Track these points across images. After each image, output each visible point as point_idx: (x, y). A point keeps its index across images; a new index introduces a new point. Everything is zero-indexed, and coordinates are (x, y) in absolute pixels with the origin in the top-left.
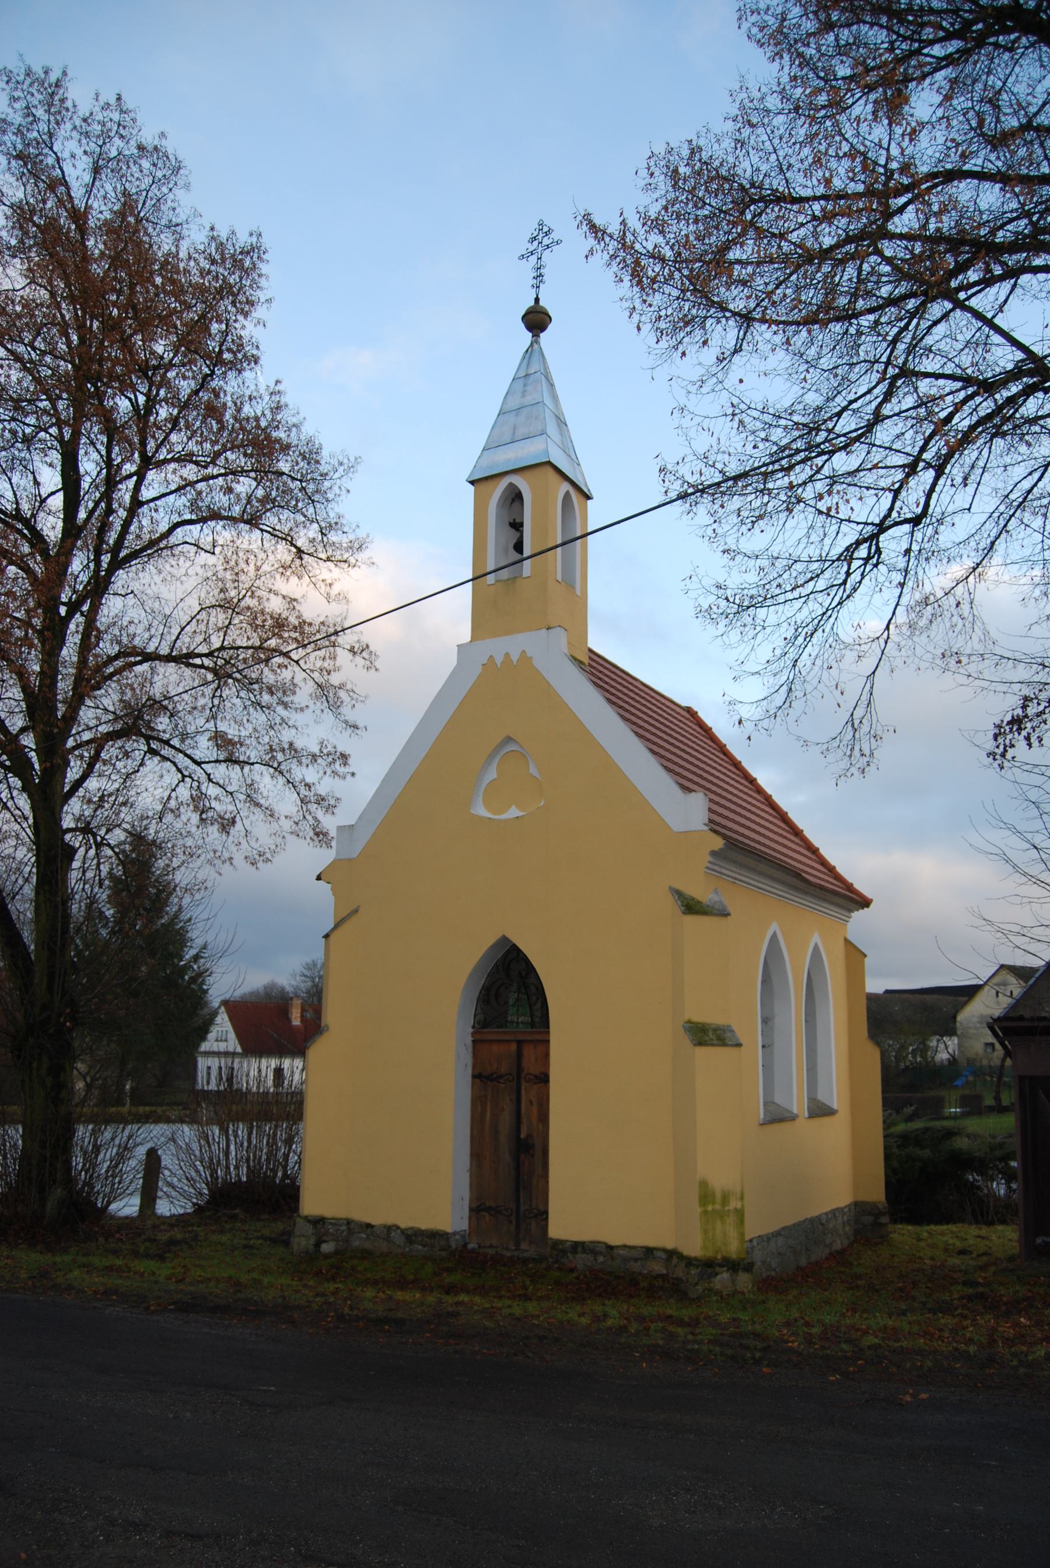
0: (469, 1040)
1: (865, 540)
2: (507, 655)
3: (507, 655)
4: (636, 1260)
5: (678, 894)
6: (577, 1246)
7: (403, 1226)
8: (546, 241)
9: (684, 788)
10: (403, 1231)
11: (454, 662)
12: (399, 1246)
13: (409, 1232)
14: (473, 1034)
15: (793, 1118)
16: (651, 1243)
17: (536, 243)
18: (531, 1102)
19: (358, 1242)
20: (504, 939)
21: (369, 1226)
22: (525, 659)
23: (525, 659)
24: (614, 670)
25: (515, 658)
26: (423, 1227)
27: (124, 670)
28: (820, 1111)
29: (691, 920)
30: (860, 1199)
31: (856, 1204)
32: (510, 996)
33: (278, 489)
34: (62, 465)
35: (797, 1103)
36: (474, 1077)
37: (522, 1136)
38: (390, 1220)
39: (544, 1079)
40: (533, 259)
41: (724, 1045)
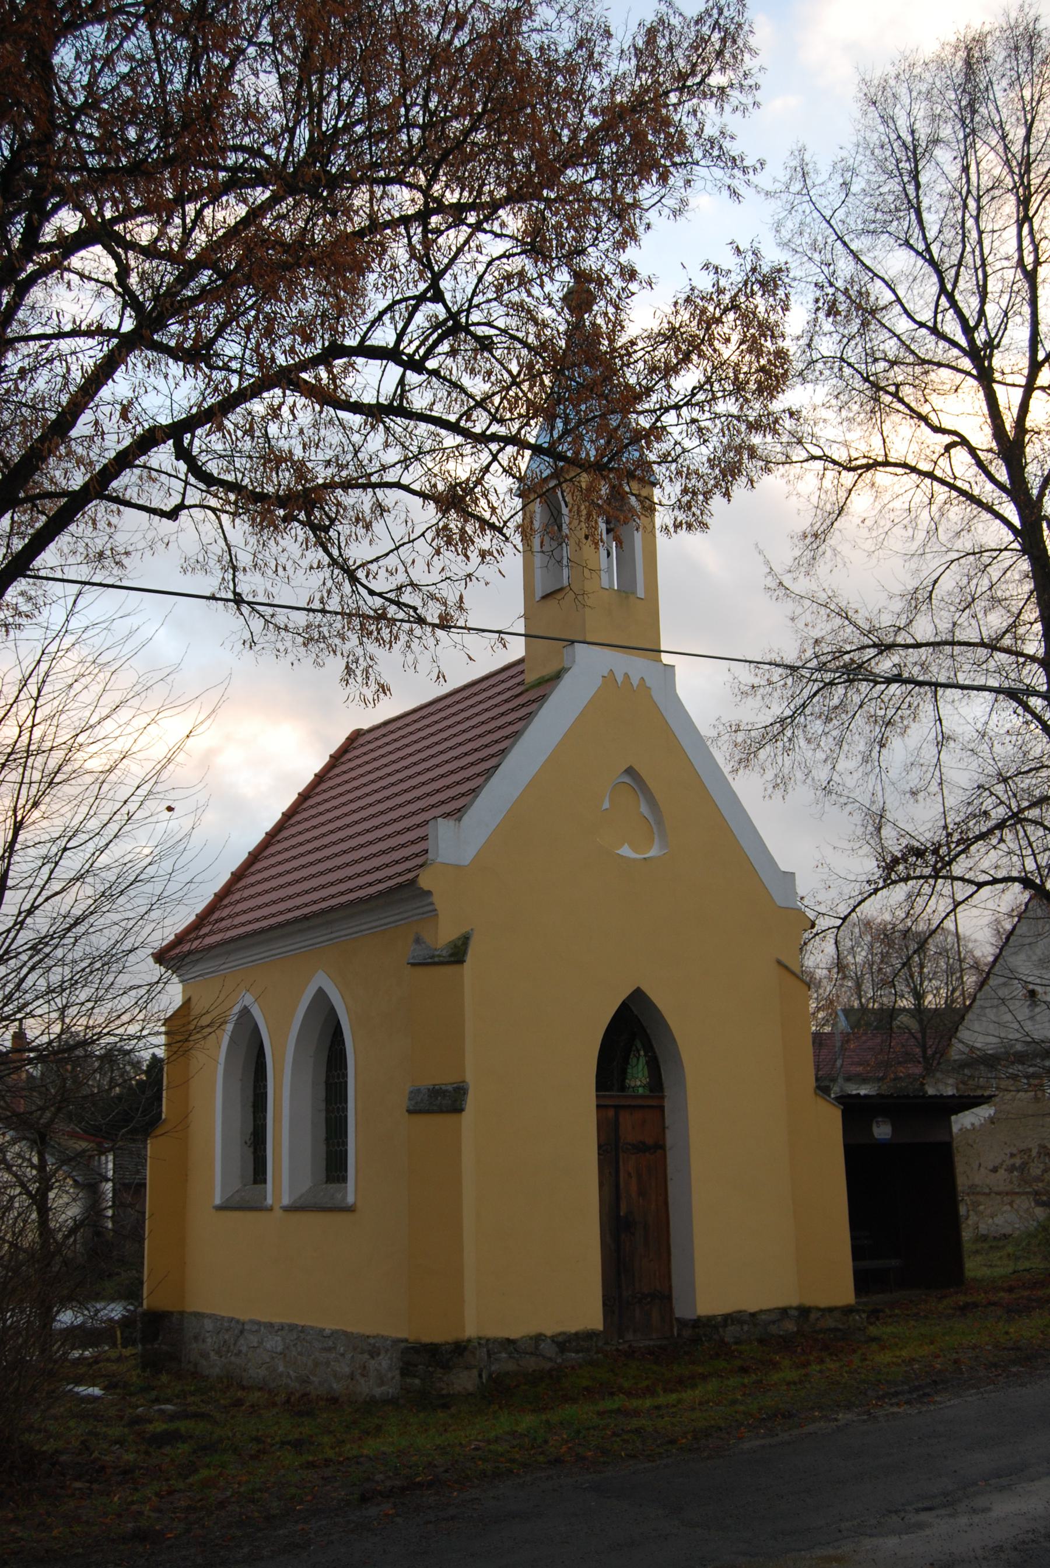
2: (626, 676)
3: (626, 676)
4: (774, 1322)
6: (729, 1319)
7: (549, 1333)
10: (553, 1339)
12: (550, 1359)
13: (560, 1339)
16: (782, 1303)
18: (629, 1174)
19: (504, 1364)
21: (509, 1341)
24: (491, 682)
25: (635, 682)
26: (573, 1330)
27: (42, 439)
32: (633, 1041)
33: (284, 318)
34: (1045, 619)
38: (532, 1329)
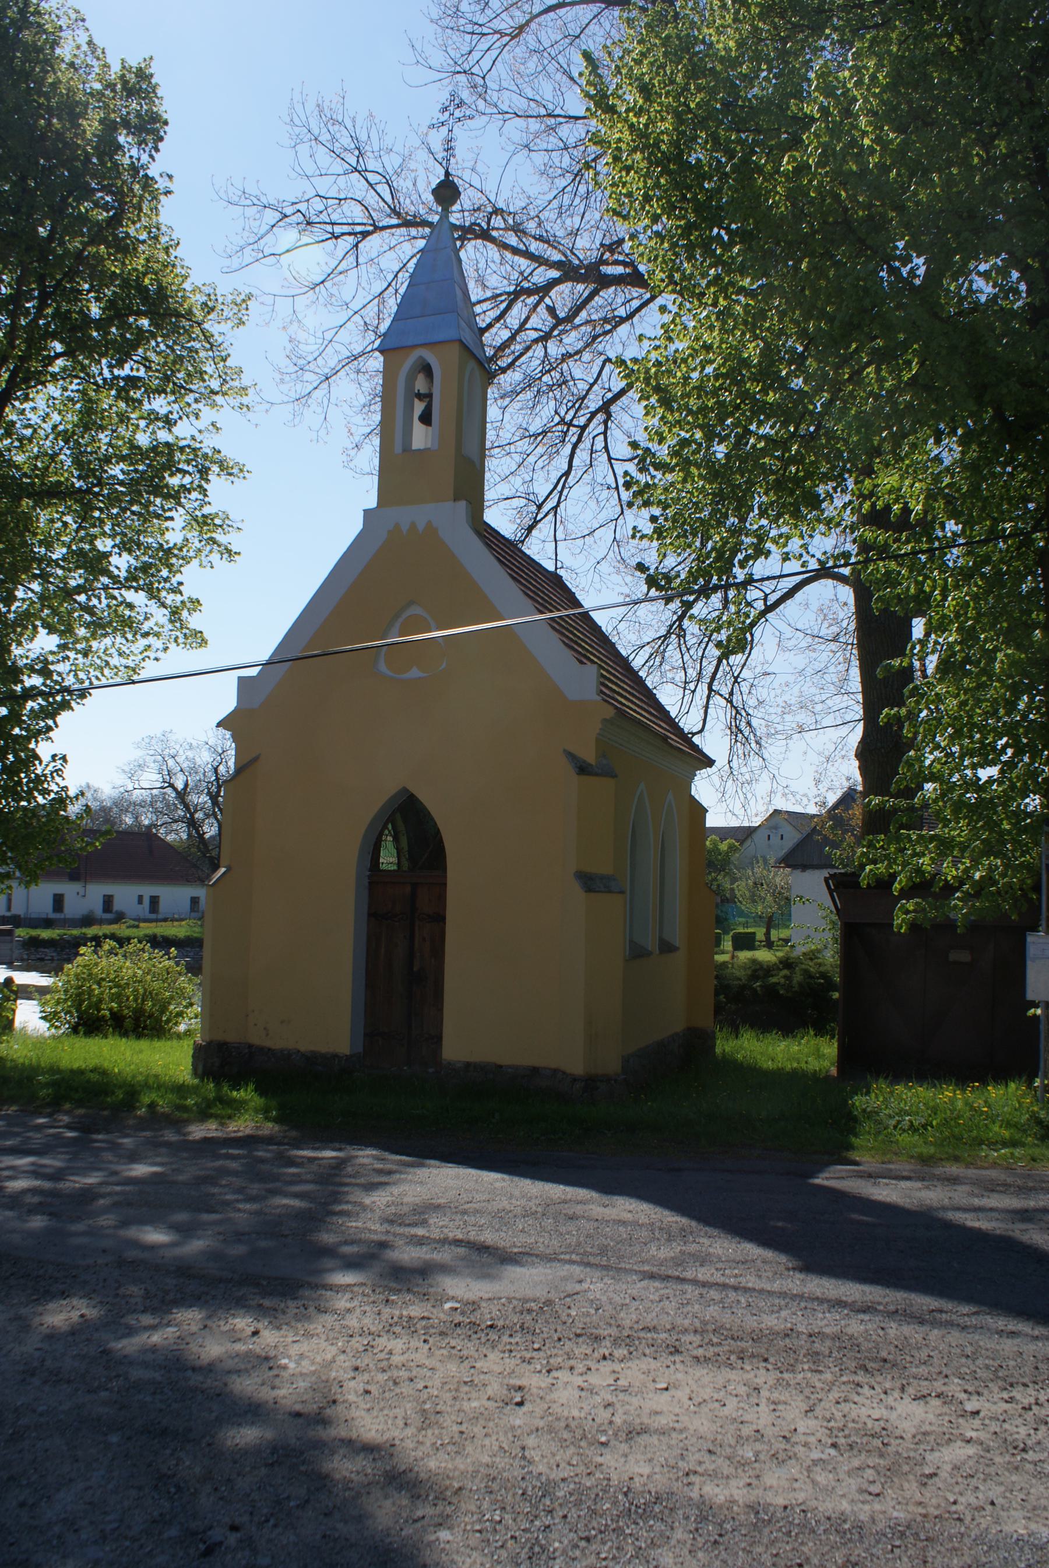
0: (366, 881)
1: (529, 292)
5: (571, 756)
8: (458, 113)
9: (581, 662)
11: (361, 527)
14: (369, 877)
15: (649, 954)
17: (447, 114)
20: (405, 790)
22: (431, 530)
23: (431, 530)
28: (667, 948)
29: (585, 778)
30: (231, 1037)
31: (210, 1043)
35: (651, 943)
36: (370, 915)
37: (415, 969)
39: (440, 919)
40: (444, 130)
41: (610, 892)
